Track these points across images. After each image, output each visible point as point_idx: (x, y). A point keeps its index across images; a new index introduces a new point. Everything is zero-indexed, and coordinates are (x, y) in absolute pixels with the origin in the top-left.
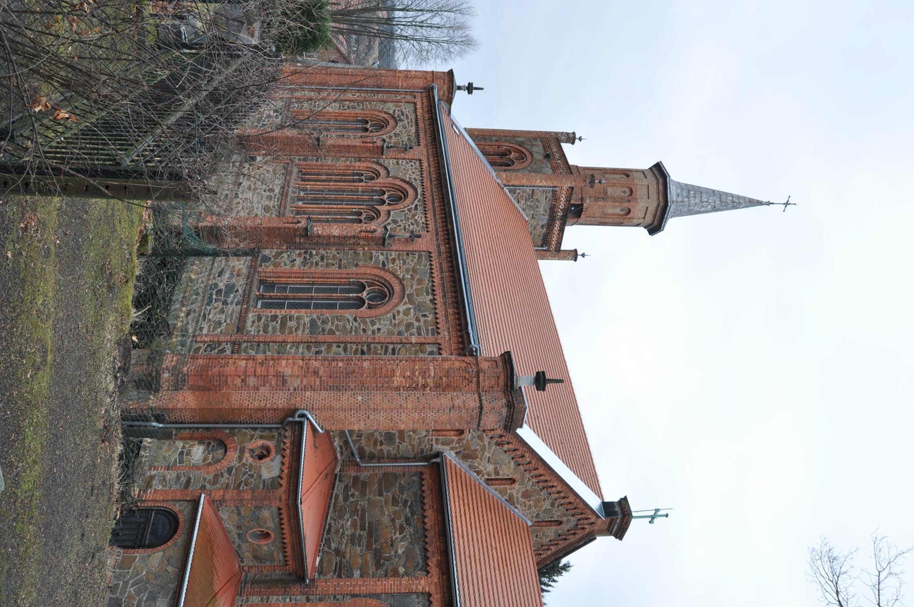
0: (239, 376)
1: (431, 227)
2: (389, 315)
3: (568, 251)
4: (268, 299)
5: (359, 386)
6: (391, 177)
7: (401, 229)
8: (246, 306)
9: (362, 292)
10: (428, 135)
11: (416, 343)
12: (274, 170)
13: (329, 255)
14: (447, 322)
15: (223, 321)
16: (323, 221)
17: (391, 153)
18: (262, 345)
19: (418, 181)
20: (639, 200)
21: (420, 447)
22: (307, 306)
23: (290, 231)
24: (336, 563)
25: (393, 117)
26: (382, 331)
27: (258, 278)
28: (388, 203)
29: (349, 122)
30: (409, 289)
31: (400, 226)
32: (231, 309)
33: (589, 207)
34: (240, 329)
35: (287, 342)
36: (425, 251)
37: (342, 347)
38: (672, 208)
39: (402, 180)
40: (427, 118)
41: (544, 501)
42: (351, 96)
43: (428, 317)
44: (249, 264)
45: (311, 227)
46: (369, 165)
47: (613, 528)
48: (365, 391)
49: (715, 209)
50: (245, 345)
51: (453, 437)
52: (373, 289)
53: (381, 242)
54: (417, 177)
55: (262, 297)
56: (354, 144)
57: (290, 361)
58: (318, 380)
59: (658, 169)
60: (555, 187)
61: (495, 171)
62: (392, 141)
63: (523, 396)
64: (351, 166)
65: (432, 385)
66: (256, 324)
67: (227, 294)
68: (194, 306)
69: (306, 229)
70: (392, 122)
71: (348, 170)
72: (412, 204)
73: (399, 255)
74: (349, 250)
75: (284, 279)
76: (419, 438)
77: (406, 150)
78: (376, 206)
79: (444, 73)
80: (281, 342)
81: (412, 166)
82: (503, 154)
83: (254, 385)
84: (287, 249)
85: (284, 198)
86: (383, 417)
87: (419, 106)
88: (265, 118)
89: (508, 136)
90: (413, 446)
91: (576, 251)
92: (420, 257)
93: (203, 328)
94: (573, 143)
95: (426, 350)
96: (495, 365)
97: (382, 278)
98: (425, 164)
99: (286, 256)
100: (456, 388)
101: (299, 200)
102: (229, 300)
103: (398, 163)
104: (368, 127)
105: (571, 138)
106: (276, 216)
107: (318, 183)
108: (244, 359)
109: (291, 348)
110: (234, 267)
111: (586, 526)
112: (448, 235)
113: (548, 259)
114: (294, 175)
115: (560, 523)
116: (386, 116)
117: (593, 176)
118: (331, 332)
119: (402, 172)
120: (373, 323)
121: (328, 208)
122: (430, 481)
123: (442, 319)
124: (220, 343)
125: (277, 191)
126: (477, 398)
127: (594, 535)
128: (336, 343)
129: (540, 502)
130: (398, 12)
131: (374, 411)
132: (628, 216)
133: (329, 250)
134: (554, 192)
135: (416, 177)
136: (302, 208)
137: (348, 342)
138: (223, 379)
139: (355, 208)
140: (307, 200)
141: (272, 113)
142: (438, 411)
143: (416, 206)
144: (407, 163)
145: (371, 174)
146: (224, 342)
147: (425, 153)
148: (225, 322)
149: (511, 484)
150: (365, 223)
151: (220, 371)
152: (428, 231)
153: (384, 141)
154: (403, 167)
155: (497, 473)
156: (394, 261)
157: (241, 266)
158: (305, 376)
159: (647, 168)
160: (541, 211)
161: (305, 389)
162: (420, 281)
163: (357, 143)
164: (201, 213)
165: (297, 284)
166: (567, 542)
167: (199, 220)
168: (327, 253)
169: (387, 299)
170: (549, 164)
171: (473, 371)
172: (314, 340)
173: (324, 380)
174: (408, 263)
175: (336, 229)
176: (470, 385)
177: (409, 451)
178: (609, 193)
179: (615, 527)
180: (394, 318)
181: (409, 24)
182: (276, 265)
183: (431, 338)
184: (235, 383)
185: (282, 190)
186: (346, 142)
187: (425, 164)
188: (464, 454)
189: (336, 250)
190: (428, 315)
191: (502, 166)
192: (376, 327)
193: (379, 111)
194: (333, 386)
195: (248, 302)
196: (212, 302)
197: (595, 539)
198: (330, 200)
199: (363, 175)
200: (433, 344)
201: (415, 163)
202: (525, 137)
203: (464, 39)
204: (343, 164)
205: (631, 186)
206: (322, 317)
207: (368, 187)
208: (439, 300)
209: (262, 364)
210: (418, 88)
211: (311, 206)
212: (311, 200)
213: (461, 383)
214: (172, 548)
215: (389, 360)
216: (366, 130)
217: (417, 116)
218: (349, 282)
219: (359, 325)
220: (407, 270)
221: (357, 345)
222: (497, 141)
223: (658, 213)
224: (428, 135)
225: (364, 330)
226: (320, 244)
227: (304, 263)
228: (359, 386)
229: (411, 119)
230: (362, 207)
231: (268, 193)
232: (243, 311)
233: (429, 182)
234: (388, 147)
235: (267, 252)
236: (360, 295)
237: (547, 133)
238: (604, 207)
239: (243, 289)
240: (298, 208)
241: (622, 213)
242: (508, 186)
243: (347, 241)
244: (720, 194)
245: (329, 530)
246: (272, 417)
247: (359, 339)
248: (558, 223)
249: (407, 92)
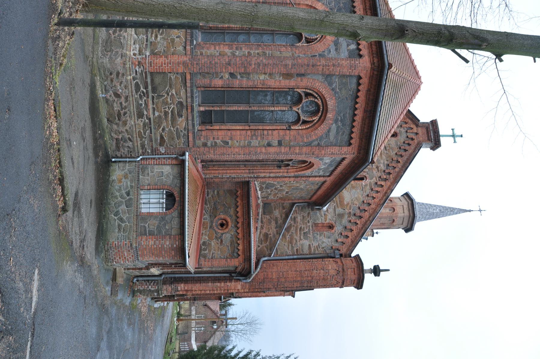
47: (431, 136)
94: (359, 285)
132: (395, 213)
159: (400, 196)
205: (393, 207)
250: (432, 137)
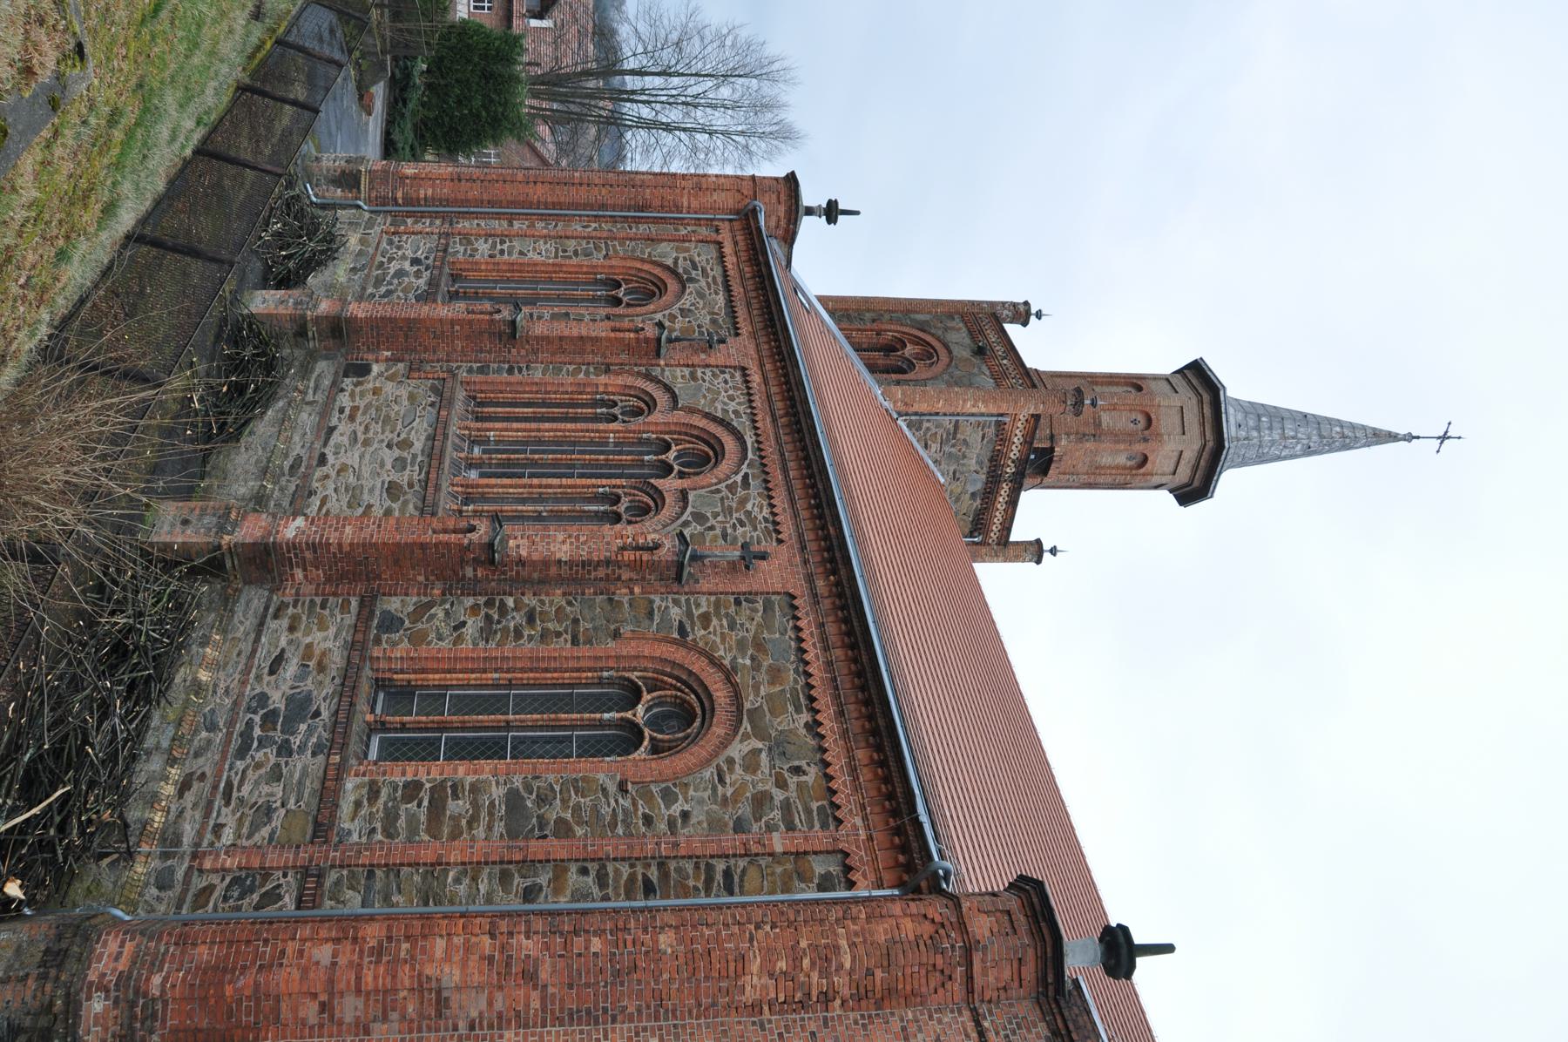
0: (314, 996)
1: (787, 530)
2: (709, 773)
3: (1022, 543)
4: (396, 730)
5: (648, 1007)
6: (681, 409)
7: (716, 536)
8: (338, 758)
9: (634, 705)
10: (755, 312)
11: (785, 853)
12: (412, 397)
13: (546, 608)
14: (857, 788)
15: (278, 804)
16: (529, 518)
17: (677, 354)
18: (379, 873)
19: (744, 418)
20: (1166, 437)
22: (493, 749)
23: (449, 551)
25: (673, 271)
26: (693, 820)
27: (370, 673)
28: (680, 472)
29: (577, 284)
30: (751, 698)
31: (712, 528)
32: (299, 766)
33: (1065, 454)
34: (322, 828)
35: (448, 864)
36: (779, 593)
37: (593, 874)
39: (707, 416)
40: (748, 275)
42: (580, 229)
43: (805, 773)
44: (350, 639)
45: (501, 541)
46: (630, 381)
48: (666, 1019)
49: (1308, 451)
50: (333, 876)
52: (660, 697)
53: (672, 573)
54: (741, 409)
55: (382, 726)
56: (594, 334)
57: (455, 939)
58: (535, 996)
59: (1198, 374)
60: (1002, 415)
61: (880, 383)
62: (677, 326)
63: (1089, 1013)
64: (589, 384)
65: (846, 992)
66: (363, 812)
67: (289, 729)
68: (201, 760)
69: (491, 545)
70: (672, 285)
71: (581, 393)
72: (736, 473)
73: (717, 605)
74: (595, 593)
75: (437, 676)
77: (711, 347)
78: (652, 481)
79: (776, 179)
80: (432, 865)
81: (726, 382)
82: (889, 349)
83: (358, 1018)
84: (443, 594)
85: (435, 463)
87: (728, 249)
88: (393, 277)
89: (895, 311)
91: (1038, 542)
92: (768, 607)
93: (223, 826)
94: (1025, 324)
95: (813, 871)
96: (1007, 924)
97: (681, 666)
98: (756, 378)
99: (441, 615)
100: (912, 998)
101: (470, 466)
102: (296, 741)
103: (693, 377)
104: (621, 295)
105: (1022, 314)
106: (416, 508)
107: (515, 425)
108: (327, 940)
109: (457, 881)
110: (309, 646)
112: (829, 549)
113: (984, 561)
114: (459, 406)
116: (657, 271)
117: (1079, 391)
118: (563, 830)
119: (705, 397)
120: (670, 799)
121: (540, 486)
123: (842, 782)
124: (266, 875)
125: (418, 446)
126: (970, 1025)
128: (577, 860)
130: (651, 78)
132: (1142, 471)
133: (547, 594)
134: (998, 423)
135: (738, 408)
136: (478, 486)
137: (608, 859)
138: (267, 1004)
139: (603, 485)
140: (490, 465)
141: (407, 265)
143: (746, 476)
144: (714, 375)
145: (634, 402)
146: (278, 868)
147: (752, 351)
148: (283, 805)
150: (630, 522)
151: (257, 985)
152: (780, 541)
153: (660, 325)
154: (707, 384)
156: (705, 619)
157: (329, 644)
158: (501, 988)
160: (972, 463)
161: (501, 1021)
162: (775, 674)
163: (601, 330)
164: (228, 509)
165: (469, 686)
167: (221, 529)
168: (542, 602)
169: (697, 724)
170: (984, 368)
171: (953, 947)
172: (518, 857)
173: (553, 995)
174: (742, 625)
175: (564, 542)
176: (948, 985)
178: (1104, 425)
180: (721, 780)
181: (672, 100)
182: (417, 639)
183: (820, 837)
184: (301, 1014)
185: (430, 443)
186: (575, 330)
187: (756, 378)
189: (564, 594)
190: (805, 767)
191: (888, 372)
192: (676, 809)
193: (643, 261)
194: (579, 1011)
195: (344, 746)
196: (249, 749)
198: (543, 466)
199: (615, 404)
200: (828, 852)
201: (733, 376)
202: (929, 313)
203: (775, 128)
204: (570, 379)
205: (1148, 409)
206: (536, 784)
207: (630, 432)
208: (829, 725)
209: (378, 952)
210: (723, 213)
211: (499, 481)
212: (498, 465)
213: (923, 981)
215: (726, 925)
216: (617, 302)
217: (725, 271)
218: (600, 678)
219: (635, 804)
220: (741, 645)
221: (632, 866)
222: (874, 321)
223: (1202, 463)
224: (755, 312)
225: (648, 820)
226: (525, 581)
227: (487, 632)
228: (648, 1007)
229: (714, 277)
230: (618, 482)
231: (397, 452)
232: (332, 773)
233: (768, 420)
234: (670, 341)
235: (393, 604)
236: (629, 715)
237: (972, 303)
238: (1096, 453)
239: (333, 707)
240: (467, 486)
241: (1129, 463)
242: (907, 414)
243: (589, 572)
244: (1319, 422)
247: (637, 848)
248: (1005, 489)
249: (699, 219)
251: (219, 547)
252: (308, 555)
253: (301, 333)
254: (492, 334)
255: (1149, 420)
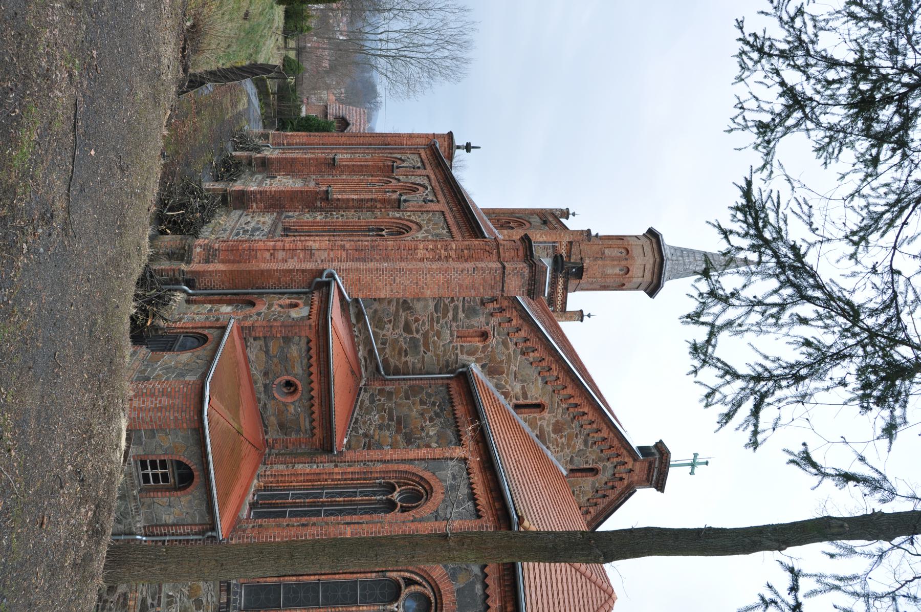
0: (268, 250)
21: (445, 358)
24: (365, 443)
38: (668, 266)
41: (576, 437)
47: (653, 476)
51: (478, 344)
59: (653, 235)
60: (554, 242)
65: (454, 256)
76: (443, 346)
86: (409, 280)
90: (437, 356)
91: (581, 311)
94: (567, 218)
111: (624, 476)
115: (594, 471)
122: (457, 388)
127: (634, 487)
129: (572, 440)
131: (400, 272)
132: (627, 276)
134: (553, 247)
142: (462, 271)
149: (541, 412)
155: (525, 396)
158: (332, 250)
166: (607, 500)
177: (434, 365)
178: (606, 254)
179: (655, 474)
188: (490, 367)
197: (636, 491)
214: (203, 351)
223: (656, 270)
241: (621, 273)
245: (356, 422)
246: (300, 281)
250: (654, 478)
251: (226, 190)
252: (258, 196)
253: (250, 164)
254: (325, 164)
255: (628, 252)
